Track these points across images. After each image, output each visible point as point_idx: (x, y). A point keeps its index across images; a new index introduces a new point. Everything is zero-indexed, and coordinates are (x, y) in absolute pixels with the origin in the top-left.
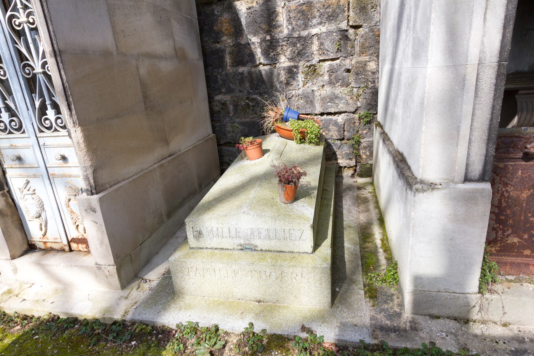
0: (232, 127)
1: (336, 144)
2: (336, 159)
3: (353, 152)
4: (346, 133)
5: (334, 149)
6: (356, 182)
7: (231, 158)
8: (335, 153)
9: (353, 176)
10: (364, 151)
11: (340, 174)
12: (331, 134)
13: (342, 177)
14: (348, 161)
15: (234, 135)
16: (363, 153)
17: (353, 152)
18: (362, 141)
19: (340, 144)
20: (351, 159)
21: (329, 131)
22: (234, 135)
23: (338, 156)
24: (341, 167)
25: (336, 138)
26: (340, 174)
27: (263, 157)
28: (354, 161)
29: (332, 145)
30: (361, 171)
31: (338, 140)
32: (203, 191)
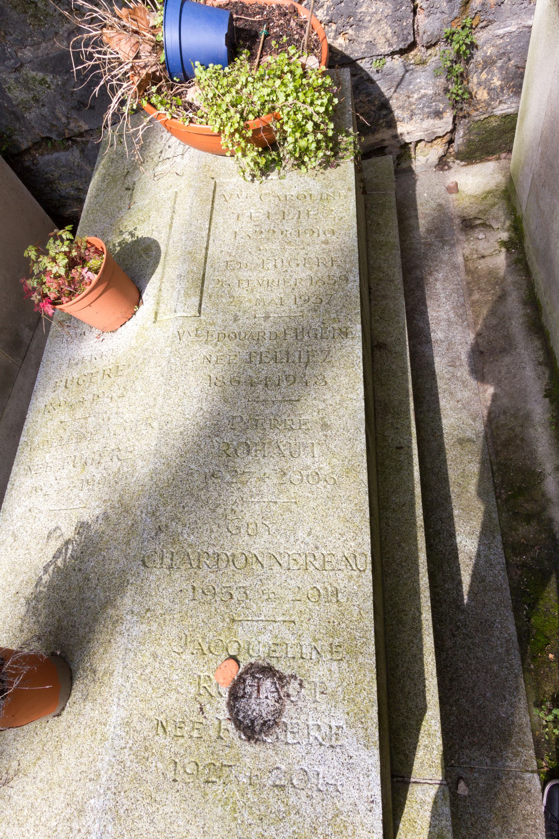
0: (26, 84)
1: (385, 72)
2: (392, 124)
3: (446, 90)
4: (420, 17)
5: (383, 89)
6: (454, 189)
7: (77, 183)
8: (385, 106)
9: (442, 164)
10: (484, 76)
11: (404, 165)
12: (366, 36)
13: (410, 171)
14: (429, 123)
15: (45, 111)
16: (479, 84)
17: (446, 90)
18: (480, 37)
19: (400, 71)
20: (438, 114)
21: (359, 25)
22: (45, 111)
23: (397, 113)
24: (407, 144)
25: (387, 50)
26: (404, 165)
27: (145, 310)
28: (448, 116)
29: (375, 77)
30: (469, 143)
31: (393, 53)
32: (33, 346)
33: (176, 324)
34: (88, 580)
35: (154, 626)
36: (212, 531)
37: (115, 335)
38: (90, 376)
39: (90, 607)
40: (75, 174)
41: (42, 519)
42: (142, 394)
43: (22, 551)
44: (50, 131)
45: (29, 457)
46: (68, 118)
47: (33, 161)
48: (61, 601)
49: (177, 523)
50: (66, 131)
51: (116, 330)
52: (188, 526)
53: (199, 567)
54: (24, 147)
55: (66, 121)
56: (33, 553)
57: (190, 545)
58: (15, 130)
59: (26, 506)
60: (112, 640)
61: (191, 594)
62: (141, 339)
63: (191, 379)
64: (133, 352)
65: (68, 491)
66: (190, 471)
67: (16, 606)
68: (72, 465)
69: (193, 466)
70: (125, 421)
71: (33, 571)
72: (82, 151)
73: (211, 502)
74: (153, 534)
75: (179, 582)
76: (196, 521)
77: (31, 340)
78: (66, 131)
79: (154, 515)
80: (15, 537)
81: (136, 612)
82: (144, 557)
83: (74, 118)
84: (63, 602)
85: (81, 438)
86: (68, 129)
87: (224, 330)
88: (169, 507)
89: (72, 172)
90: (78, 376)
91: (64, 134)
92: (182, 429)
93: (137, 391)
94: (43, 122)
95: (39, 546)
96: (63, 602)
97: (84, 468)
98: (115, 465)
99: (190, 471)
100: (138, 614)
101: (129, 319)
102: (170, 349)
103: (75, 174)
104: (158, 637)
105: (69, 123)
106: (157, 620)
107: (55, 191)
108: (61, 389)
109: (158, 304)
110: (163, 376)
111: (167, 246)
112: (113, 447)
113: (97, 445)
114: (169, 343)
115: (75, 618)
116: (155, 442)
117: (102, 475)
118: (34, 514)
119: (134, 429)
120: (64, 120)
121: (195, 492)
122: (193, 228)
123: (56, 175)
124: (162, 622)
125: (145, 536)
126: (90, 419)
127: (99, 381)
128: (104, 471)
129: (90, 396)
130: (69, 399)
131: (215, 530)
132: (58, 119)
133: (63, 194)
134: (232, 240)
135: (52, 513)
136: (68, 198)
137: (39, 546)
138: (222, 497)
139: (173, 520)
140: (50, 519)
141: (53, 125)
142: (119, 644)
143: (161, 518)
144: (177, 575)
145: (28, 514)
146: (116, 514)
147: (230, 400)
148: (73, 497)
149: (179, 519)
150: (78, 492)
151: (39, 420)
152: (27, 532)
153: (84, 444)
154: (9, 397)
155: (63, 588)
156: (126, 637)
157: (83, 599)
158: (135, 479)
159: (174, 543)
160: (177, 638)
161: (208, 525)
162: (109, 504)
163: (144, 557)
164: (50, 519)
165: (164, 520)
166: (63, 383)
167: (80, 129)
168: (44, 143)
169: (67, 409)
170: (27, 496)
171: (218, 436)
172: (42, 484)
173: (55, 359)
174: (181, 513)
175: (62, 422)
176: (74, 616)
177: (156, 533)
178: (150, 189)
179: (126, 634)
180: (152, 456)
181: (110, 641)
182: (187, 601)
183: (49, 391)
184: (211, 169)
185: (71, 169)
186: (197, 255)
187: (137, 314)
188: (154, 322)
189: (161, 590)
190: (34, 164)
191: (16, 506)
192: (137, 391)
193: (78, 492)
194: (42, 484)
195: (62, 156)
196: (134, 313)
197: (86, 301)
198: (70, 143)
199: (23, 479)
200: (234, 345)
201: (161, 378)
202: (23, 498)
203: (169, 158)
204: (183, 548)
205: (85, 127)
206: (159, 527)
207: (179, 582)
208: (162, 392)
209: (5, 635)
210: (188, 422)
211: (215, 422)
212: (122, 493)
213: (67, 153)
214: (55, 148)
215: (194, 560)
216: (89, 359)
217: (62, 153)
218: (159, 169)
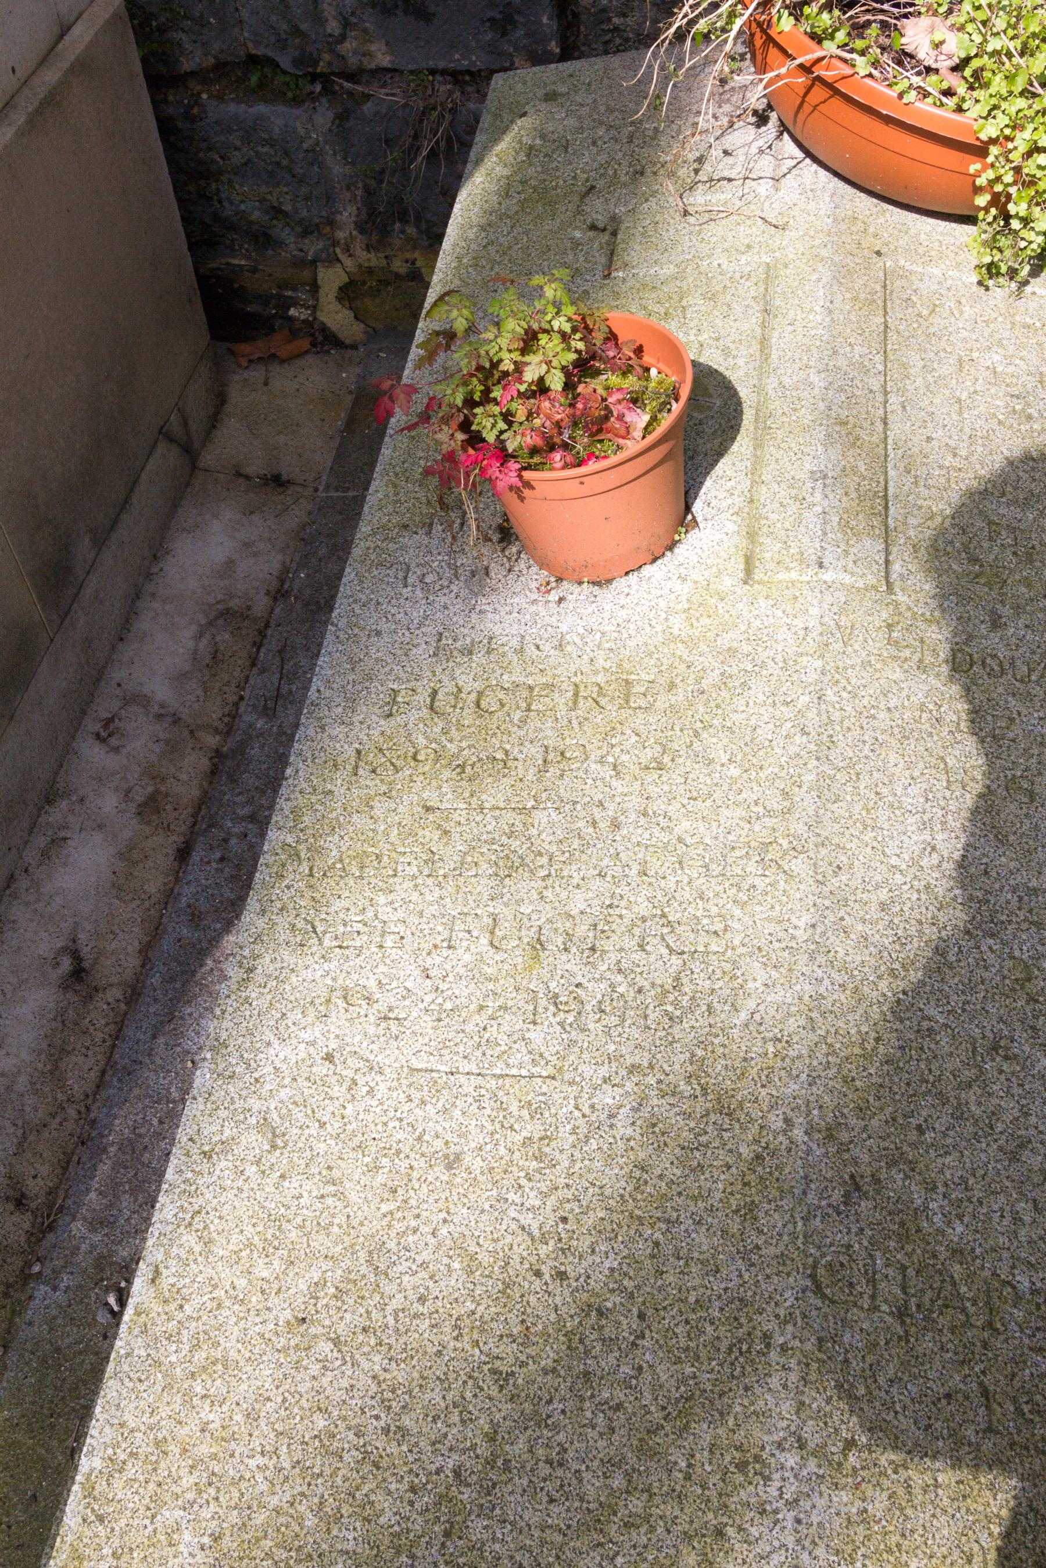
33: (829, 599)
34: (600, 1313)
35: (878, 1506)
36: (1017, 1220)
37: (606, 595)
38: (525, 694)
39: (619, 1407)
40: (290, 171)
41: (382, 1089)
42: (734, 771)
43: (308, 1185)
44: (282, 44)
45: (308, 894)
46: (346, 25)
47: (190, 106)
48: (494, 1371)
49: (906, 1177)
50: (326, 57)
51: (609, 581)
52: (941, 1189)
53: (990, 1325)
54: (187, 65)
55: (337, 32)
56: (353, 1197)
57: (956, 1252)
58: (185, 17)
59: (312, 1043)
60: (730, 1531)
61: (982, 1411)
62: (704, 621)
63: (893, 758)
64: (681, 650)
65: (481, 1019)
66: (925, 1024)
67: (297, 1366)
68: (484, 941)
69: (931, 1011)
70: (680, 840)
71: (362, 1255)
72: (342, 117)
73: (1000, 1127)
74: (837, 1196)
75: (938, 1365)
76: (964, 1180)
77: (88, 573)
78: (326, 57)
79: (830, 1137)
80: (275, 1138)
81: (811, 1445)
82: (815, 1267)
83: (365, 31)
84: (503, 1379)
85: (510, 866)
86: (332, 51)
87: (966, 644)
88: (875, 1122)
89: (285, 162)
90: (478, 685)
91: (316, 64)
92: (883, 895)
93: (711, 761)
94: (274, 18)
95: (381, 1178)
96: (503, 1379)
97: (536, 958)
98: (660, 967)
99: (925, 1024)
100: (819, 1452)
101: (654, 560)
102: (819, 663)
103: (290, 171)
104: (895, 1539)
105: (343, 38)
106: (886, 1483)
107: (210, 199)
108: (413, 716)
109: (752, 535)
110: (804, 732)
111: (758, 389)
112: (643, 908)
113: (579, 896)
114: (810, 646)
115: (561, 1437)
116: (806, 919)
117: (613, 987)
118: (349, 1073)
119: (716, 869)
120: (333, 27)
121: (948, 1088)
122: (842, 362)
123: (237, 158)
124: (901, 1492)
125: (812, 1198)
126: (538, 815)
127: (562, 712)
128: (620, 978)
129: (534, 751)
130: (452, 748)
131: (1027, 1219)
132: (319, 20)
133: (228, 211)
134: (955, 417)
135: (422, 1079)
136: (233, 228)
137: (381, 1178)
138: (1033, 1120)
139: (892, 1163)
140: (416, 1096)
141: (296, 31)
142: (763, 1547)
143: (856, 1151)
144: (927, 1344)
145: (322, 1069)
146: (687, 1115)
147: (1011, 838)
148: (503, 1039)
149: (912, 1165)
150: (520, 1025)
151: (340, 791)
152: (322, 1125)
153: (524, 886)
154: (12, 718)
155: (498, 1328)
156: (789, 1524)
157: (586, 1374)
158: (743, 1016)
159: (904, 1238)
160: (956, 1553)
161: (1002, 1199)
162: (651, 1080)
163: (815, 1267)
164: (416, 1096)
165: (866, 1158)
166: (423, 697)
167: (365, 61)
168: (248, 72)
169: (447, 774)
170: (311, 1013)
171: (992, 935)
172: (372, 984)
173: (383, 626)
174: (913, 1145)
175: (428, 809)
176: (556, 1428)
177: (847, 1195)
178: (674, 243)
179: (788, 1517)
180: (803, 958)
181: (720, 1533)
182: (969, 1432)
183: (368, 712)
184: (872, 230)
185: (286, 153)
186: (862, 434)
187: (679, 550)
188: (745, 583)
189: (881, 1381)
190: (188, 117)
191: (269, 1036)
192: (711, 761)
193: (520, 1025)
194: (372, 984)
195: (276, 116)
196: (671, 547)
197: (614, 478)
198: (318, 88)
199: (288, 957)
200: (1000, 690)
201: (799, 739)
202: (295, 1016)
203: (730, 180)
204: (935, 1256)
205: (384, 60)
206: (852, 1177)
207: (938, 1365)
208: (809, 778)
209: (260, 1460)
210: (899, 878)
211: (979, 894)
212: (700, 1053)
213: (296, 112)
214: (263, 92)
215: (974, 1303)
216: (514, 643)
217: (282, 109)
218: (699, 199)
